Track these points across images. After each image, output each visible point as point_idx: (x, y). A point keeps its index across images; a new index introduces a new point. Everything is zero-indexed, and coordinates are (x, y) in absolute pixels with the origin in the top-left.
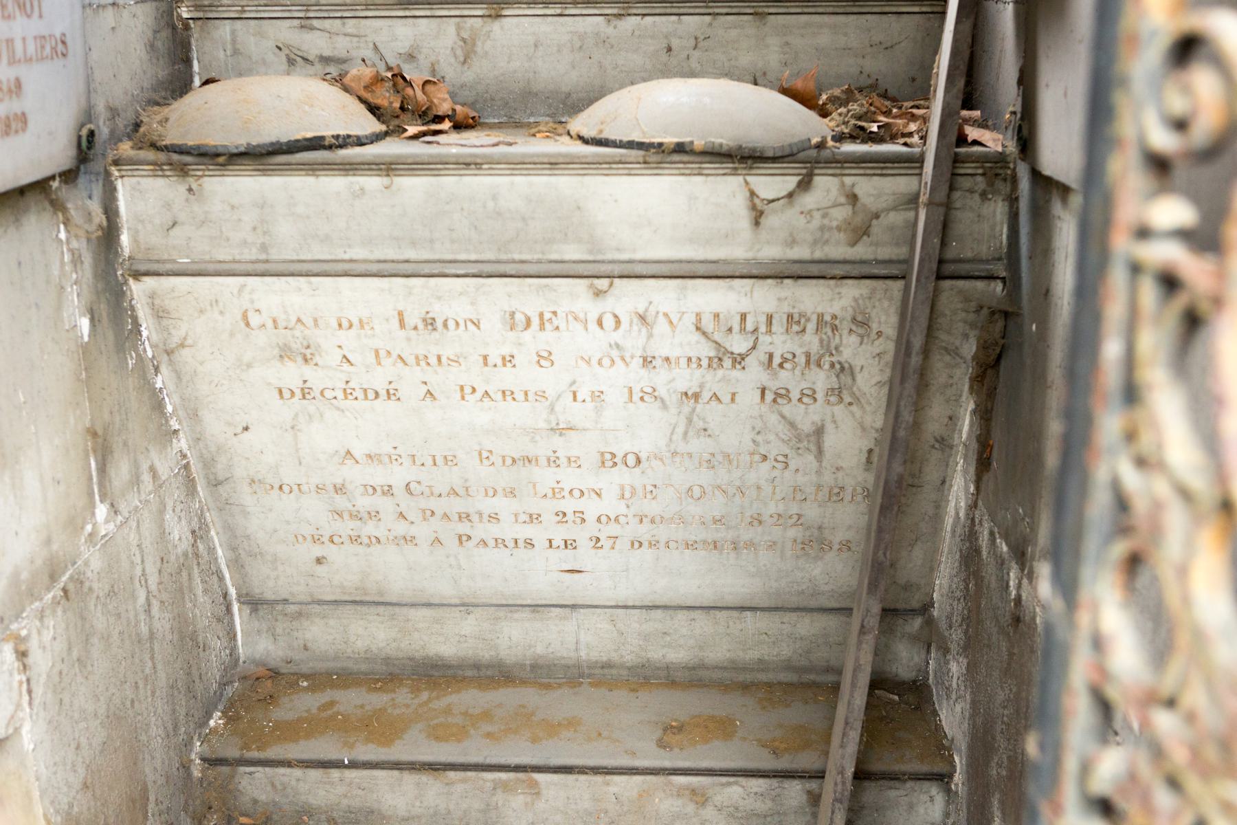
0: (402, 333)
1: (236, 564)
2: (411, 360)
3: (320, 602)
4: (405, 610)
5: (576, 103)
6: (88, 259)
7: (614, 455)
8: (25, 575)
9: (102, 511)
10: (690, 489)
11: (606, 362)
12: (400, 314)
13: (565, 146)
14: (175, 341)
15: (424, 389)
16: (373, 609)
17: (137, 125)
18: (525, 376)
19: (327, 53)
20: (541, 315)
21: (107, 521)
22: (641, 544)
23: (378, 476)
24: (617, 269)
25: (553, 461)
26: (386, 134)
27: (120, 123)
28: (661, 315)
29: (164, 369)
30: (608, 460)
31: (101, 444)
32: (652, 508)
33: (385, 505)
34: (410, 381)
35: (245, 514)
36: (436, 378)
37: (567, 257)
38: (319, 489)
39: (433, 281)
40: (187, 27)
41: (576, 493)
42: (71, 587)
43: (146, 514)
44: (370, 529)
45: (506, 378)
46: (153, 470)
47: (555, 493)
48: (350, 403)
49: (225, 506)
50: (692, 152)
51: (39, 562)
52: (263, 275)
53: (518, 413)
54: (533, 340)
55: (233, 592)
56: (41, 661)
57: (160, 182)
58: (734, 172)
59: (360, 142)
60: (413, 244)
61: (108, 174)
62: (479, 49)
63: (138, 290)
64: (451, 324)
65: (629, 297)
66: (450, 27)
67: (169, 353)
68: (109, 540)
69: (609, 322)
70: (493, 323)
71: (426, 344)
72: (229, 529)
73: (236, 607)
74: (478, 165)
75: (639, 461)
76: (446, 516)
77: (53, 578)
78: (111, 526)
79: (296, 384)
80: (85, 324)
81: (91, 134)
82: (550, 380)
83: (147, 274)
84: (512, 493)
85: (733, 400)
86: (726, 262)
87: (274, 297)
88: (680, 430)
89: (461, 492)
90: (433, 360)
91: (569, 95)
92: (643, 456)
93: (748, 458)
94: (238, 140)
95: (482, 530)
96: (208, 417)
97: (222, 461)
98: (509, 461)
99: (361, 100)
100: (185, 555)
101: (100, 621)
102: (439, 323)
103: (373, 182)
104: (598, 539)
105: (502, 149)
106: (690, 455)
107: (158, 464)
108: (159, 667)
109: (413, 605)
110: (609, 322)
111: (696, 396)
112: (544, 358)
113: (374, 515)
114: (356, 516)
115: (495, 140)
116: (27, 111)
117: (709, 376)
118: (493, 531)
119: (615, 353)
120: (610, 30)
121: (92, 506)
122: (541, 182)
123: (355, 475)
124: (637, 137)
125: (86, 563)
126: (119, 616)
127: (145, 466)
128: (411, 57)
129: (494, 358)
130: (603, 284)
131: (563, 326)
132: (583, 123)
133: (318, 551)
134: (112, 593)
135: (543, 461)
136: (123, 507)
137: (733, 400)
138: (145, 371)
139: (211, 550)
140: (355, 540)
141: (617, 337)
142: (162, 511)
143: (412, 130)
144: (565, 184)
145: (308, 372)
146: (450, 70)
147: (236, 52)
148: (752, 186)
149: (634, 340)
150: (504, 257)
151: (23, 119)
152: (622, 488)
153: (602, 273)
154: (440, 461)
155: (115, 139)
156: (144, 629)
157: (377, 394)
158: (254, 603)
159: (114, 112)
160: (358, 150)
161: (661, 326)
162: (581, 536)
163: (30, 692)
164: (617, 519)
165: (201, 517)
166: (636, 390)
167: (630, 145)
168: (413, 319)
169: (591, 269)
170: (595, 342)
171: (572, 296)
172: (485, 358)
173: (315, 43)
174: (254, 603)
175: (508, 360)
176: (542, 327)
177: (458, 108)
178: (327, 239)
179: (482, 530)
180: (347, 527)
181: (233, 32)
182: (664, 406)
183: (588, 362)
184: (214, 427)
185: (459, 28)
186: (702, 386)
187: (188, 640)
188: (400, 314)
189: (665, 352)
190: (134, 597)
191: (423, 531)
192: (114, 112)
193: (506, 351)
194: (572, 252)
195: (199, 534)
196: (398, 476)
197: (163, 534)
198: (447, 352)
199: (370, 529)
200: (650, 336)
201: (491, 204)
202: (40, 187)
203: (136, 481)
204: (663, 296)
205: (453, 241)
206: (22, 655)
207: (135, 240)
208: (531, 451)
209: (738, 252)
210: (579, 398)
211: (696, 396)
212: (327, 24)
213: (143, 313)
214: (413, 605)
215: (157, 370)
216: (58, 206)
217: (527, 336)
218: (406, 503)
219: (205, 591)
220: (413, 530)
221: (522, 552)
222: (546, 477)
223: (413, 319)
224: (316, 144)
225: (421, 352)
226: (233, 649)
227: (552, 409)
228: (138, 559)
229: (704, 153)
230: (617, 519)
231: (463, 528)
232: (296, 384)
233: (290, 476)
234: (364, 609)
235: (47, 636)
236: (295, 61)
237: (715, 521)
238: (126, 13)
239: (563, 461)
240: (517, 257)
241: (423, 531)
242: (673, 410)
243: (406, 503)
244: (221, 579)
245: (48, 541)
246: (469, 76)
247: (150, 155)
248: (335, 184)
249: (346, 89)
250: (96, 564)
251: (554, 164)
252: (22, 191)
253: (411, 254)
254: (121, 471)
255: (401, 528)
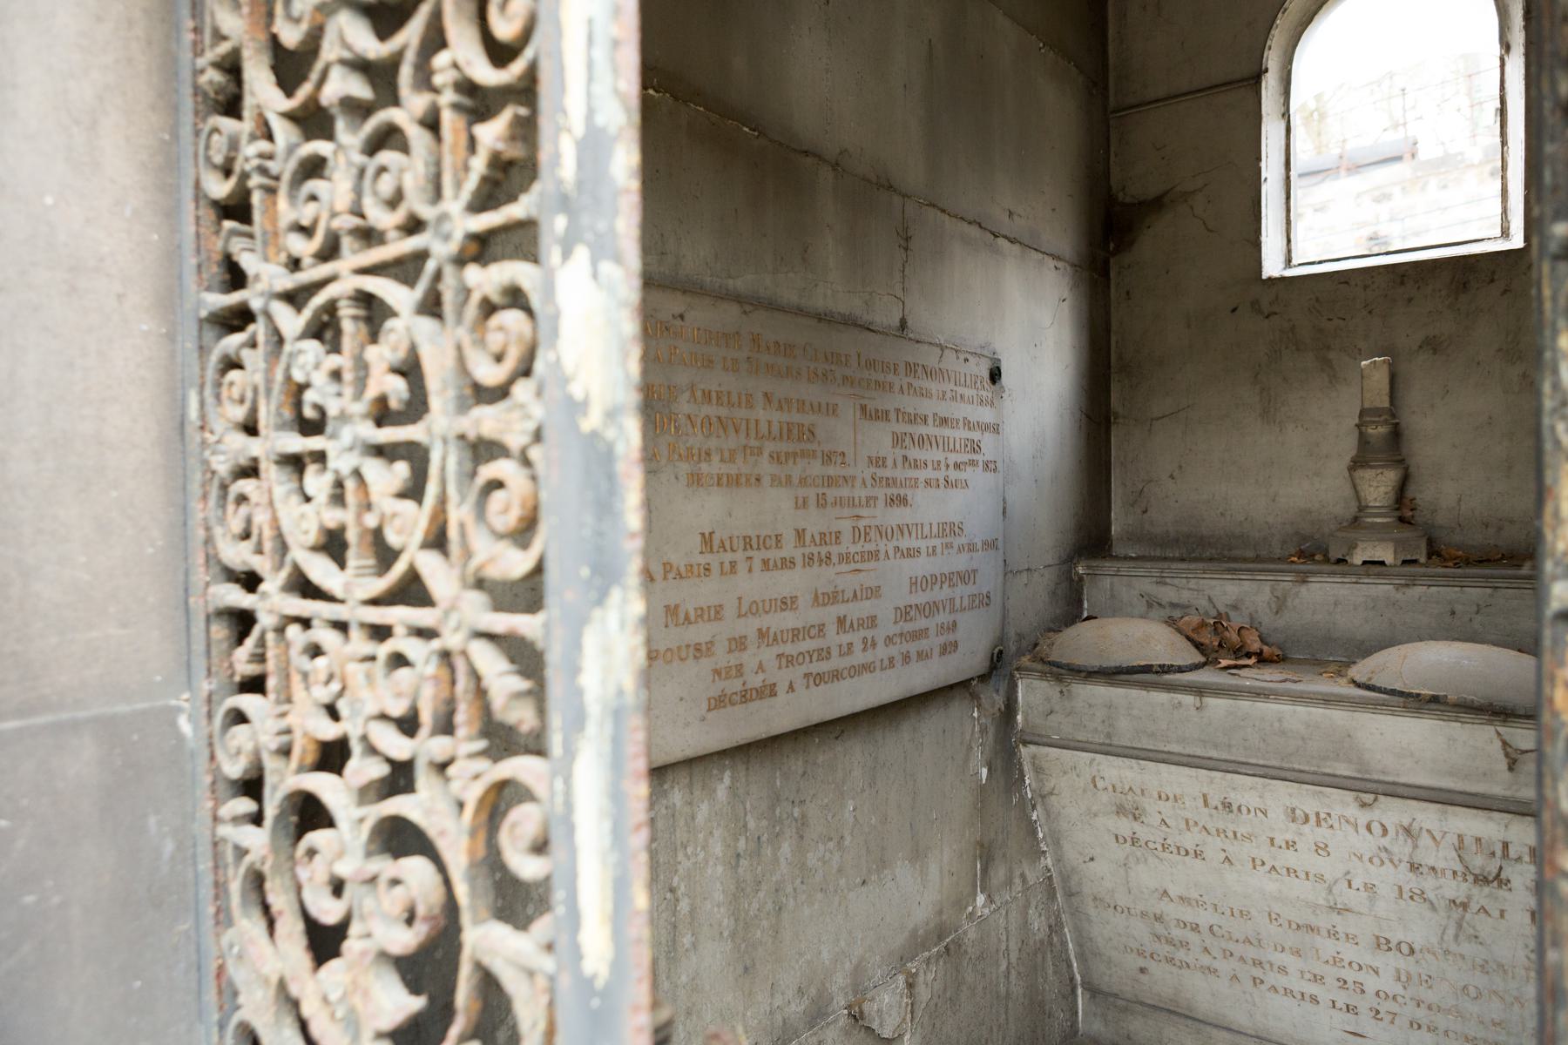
0: (1206, 810)
1: (1082, 957)
2: (1213, 831)
3: (1142, 1004)
4: (1208, 1028)
5: (1366, 649)
6: (991, 730)
7: (1388, 941)
8: (921, 932)
9: (981, 899)
10: (1465, 987)
11: (1376, 860)
12: (1205, 796)
13: (1342, 688)
14: (1047, 789)
15: (1223, 855)
16: (1182, 1020)
17: (1036, 645)
18: (1303, 859)
19: (1175, 601)
20: (1317, 814)
21: (984, 906)
22: (1419, 1027)
23: (1188, 915)
24: (1381, 788)
25: (1333, 934)
26: (1205, 664)
27: (1024, 644)
28: (1424, 833)
29: (1039, 807)
30: (1382, 944)
31: (986, 854)
32: (1429, 996)
33: (1192, 937)
34: (1213, 847)
35: (1089, 921)
36: (1233, 849)
37: (1338, 772)
38: (1143, 914)
39: (1229, 776)
40: (1081, 579)
41: (1355, 966)
42: (952, 947)
43: (1014, 906)
44: (1181, 955)
45: (1289, 858)
46: (1023, 876)
47: (1336, 961)
48: (1166, 855)
49: (1076, 912)
50: (1446, 704)
51: (932, 925)
52: (1107, 754)
53: (1299, 888)
54: (1311, 833)
55: (1078, 977)
56: (923, 993)
57: (1044, 684)
58: (1490, 723)
59: (1180, 670)
60: (1216, 746)
61: (1012, 676)
62: (1289, 603)
63: (1025, 752)
64: (1244, 809)
65: (1393, 812)
66: (1267, 588)
67: (1043, 797)
68: (984, 920)
69: (1376, 828)
70: (1277, 815)
71: (1222, 821)
72: (1078, 931)
73: (1080, 991)
74: (1267, 696)
75: (1412, 951)
76: (1242, 958)
77: (940, 938)
78: (986, 911)
79: (1128, 834)
80: (985, 771)
81: (1001, 652)
82: (1329, 867)
83: (1031, 743)
84: (1297, 953)
85: (1502, 916)
86: (1483, 796)
87: (1115, 770)
88: (1451, 932)
89: (1255, 942)
90: (1230, 835)
91: (1363, 642)
92: (1416, 947)
93: (1523, 972)
94: (1094, 662)
95: (1272, 978)
96: (1066, 845)
97: (1075, 878)
98: (1294, 926)
99: (1188, 638)
100: (1042, 942)
101: (969, 977)
102: (1235, 808)
103: (1189, 699)
104: (1378, 1012)
105: (1289, 685)
106: (1463, 957)
107: (1027, 873)
108: (1011, 1020)
109: (1216, 1026)
110: (1376, 828)
111: (1465, 906)
112: (1321, 849)
113: (1185, 944)
114: (1170, 942)
115: (1284, 676)
116: (288, 977)
117: (1476, 891)
118: (1281, 981)
119: (1384, 855)
120: (1399, 596)
121: (975, 895)
122: (1318, 712)
123: (1172, 911)
124: (1398, 686)
125: (965, 933)
126: (984, 975)
127: (1017, 873)
128: (1235, 607)
129: (1279, 841)
130: (1369, 798)
131: (1336, 825)
132: (1360, 671)
133: (1141, 963)
134: (981, 958)
135: (1324, 933)
136: (996, 898)
137: (1502, 916)
138: (1025, 807)
139: (1064, 943)
140: (1170, 960)
141: (1385, 842)
142: (1027, 906)
143: (1224, 663)
144: (1338, 716)
145: (1137, 826)
146: (1267, 620)
147: (1113, 596)
148: (1506, 738)
149: (1402, 848)
150: (1286, 765)
151: (955, 645)
152: (1398, 971)
153: (1371, 788)
154: (1236, 913)
155: (1020, 653)
156: (1002, 989)
157: (1187, 853)
158: (1093, 991)
159: (1020, 636)
160: (1178, 676)
161: (1425, 840)
162: (1363, 1005)
163: (912, 1012)
164: (1394, 997)
165: (1058, 916)
166: (1406, 889)
167: (1393, 692)
168: (1215, 801)
169: (1358, 784)
170: (1367, 844)
171: (1342, 804)
172: (1272, 840)
173: (1167, 594)
174: (1093, 991)
175: (1290, 845)
176: (1318, 824)
177: (1265, 648)
178: (1152, 735)
179: (1272, 978)
180: (1164, 949)
181: (1112, 584)
182: (1433, 908)
183: (1360, 858)
184: (1070, 854)
185: (1273, 590)
186: (1469, 897)
187: (1036, 1006)
188: (1205, 796)
189: (1431, 862)
190: (998, 965)
191: (1224, 966)
192: (1020, 636)
193: (1289, 837)
194: (1343, 769)
195: (1055, 928)
196: (1204, 918)
197: (1025, 924)
198: (1241, 830)
199: (1181, 955)
200: (1415, 847)
201: (1276, 725)
202: (964, 685)
203: (1009, 882)
204: (1427, 816)
205: (1245, 748)
206: (910, 986)
207: (1026, 719)
208: (1314, 921)
209: (1497, 788)
210: (1354, 886)
211: (1465, 906)
212: (1176, 581)
213: (1027, 768)
214: (1216, 1026)
215: (1034, 807)
216: (975, 697)
217: (1306, 828)
218: (1209, 941)
219: (1055, 973)
220: (1216, 964)
221: (1307, 1005)
222: (1328, 947)
223: (1215, 801)
224: (1147, 669)
225: (1221, 826)
226: (1074, 1023)
227: (1330, 890)
228: (1004, 938)
229: (1455, 705)
230: (1394, 997)
231: (1257, 972)
232: (1128, 834)
233: (1122, 900)
234: (1175, 1018)
235: (930, 977)
236: (1152, 603)
237: (1494, 1024)
238: (1036, 575)
239: (1342, 936)
240: (1297, 766)
241: (1224, 966)
242: (1443, 914)
243: (1209, 941)
244: (1070, 966)
245: (940, 912)
246: (1280, 623)
247: (1039, 666)
248: (1162, 697)
249: (1179, 631)
250: (972, 934)
251: (1327, 701)
252: (951, 687)
253: (1214, 754)
254: (999, 874)
255: (1206, 960)
